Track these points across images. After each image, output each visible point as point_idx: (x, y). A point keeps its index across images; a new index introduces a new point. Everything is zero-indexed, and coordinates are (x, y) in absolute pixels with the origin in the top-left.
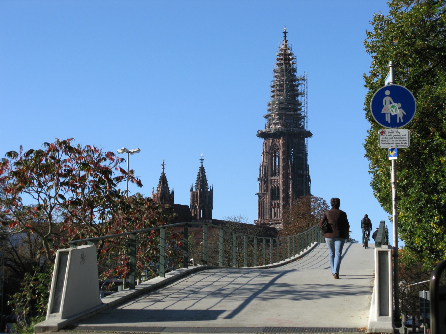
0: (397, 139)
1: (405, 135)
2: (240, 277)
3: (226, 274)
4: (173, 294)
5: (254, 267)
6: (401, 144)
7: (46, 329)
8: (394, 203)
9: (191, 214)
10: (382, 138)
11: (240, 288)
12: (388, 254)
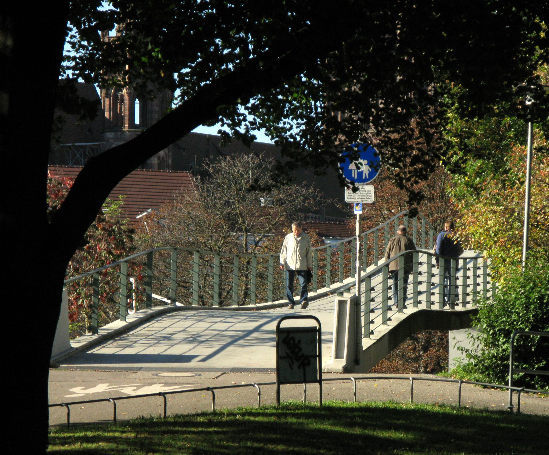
0: (362, 195)
1: (370, 191)
2: (221, 321)
3: (201, 318)
4: (141, 340)
6: (366, 199)
8: (358, 255)
9: (104, 112)
10: (349, 193)
11: (218, 334)
12: (347, 303)
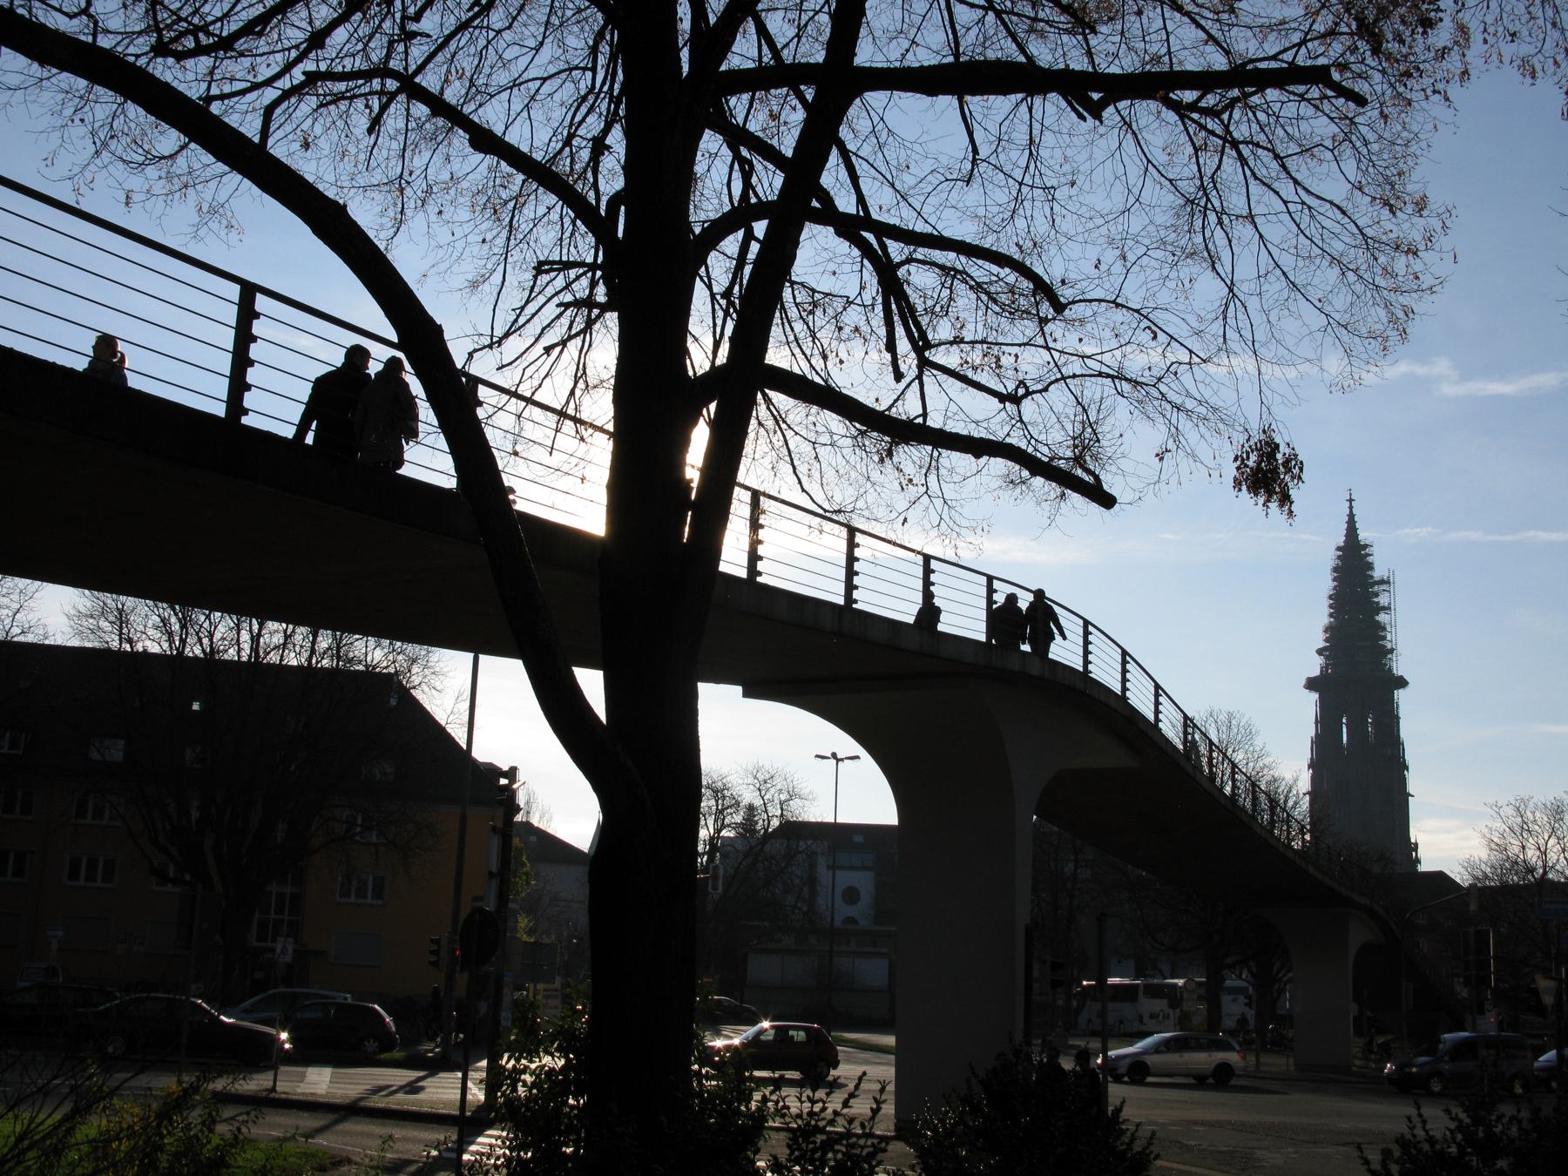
5: (620, 72)
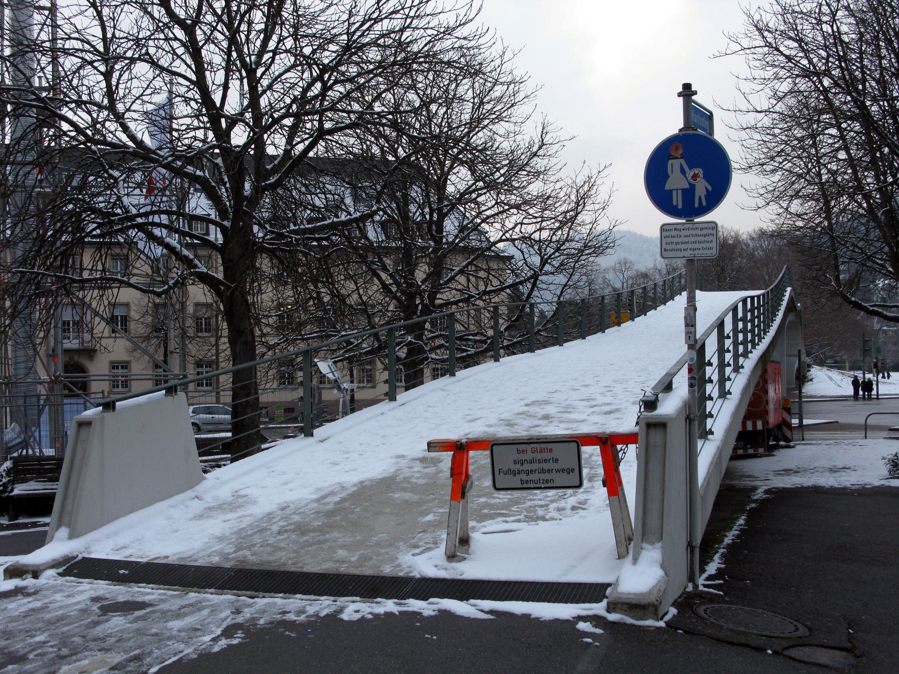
7: (130, 672)
